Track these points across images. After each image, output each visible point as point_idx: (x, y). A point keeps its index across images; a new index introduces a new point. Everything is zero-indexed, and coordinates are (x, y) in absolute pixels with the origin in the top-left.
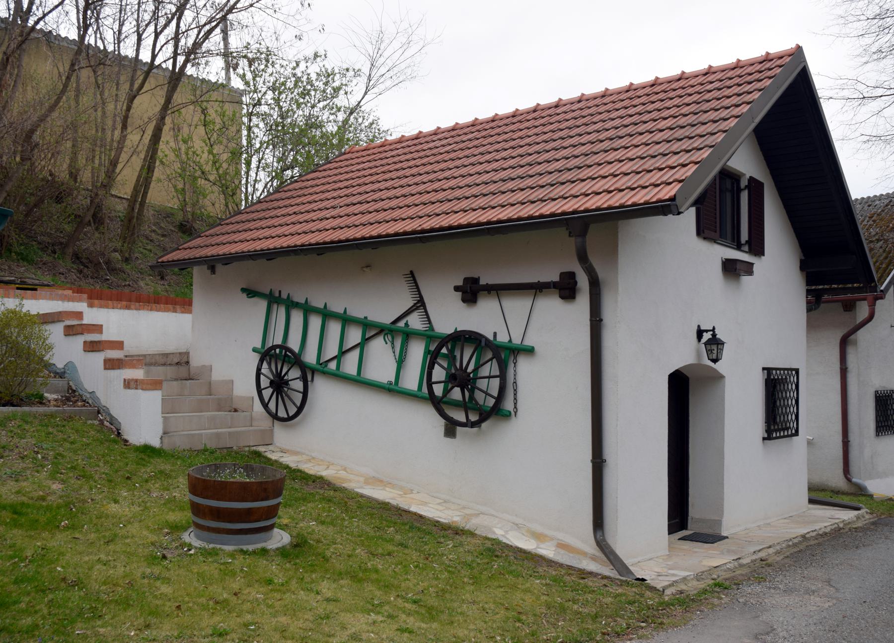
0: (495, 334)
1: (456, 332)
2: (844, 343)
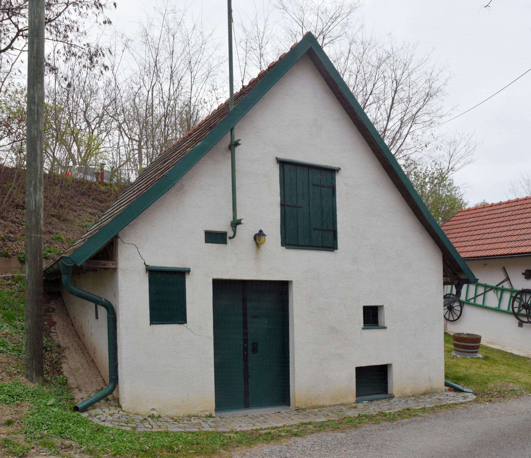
1: (523, 289)
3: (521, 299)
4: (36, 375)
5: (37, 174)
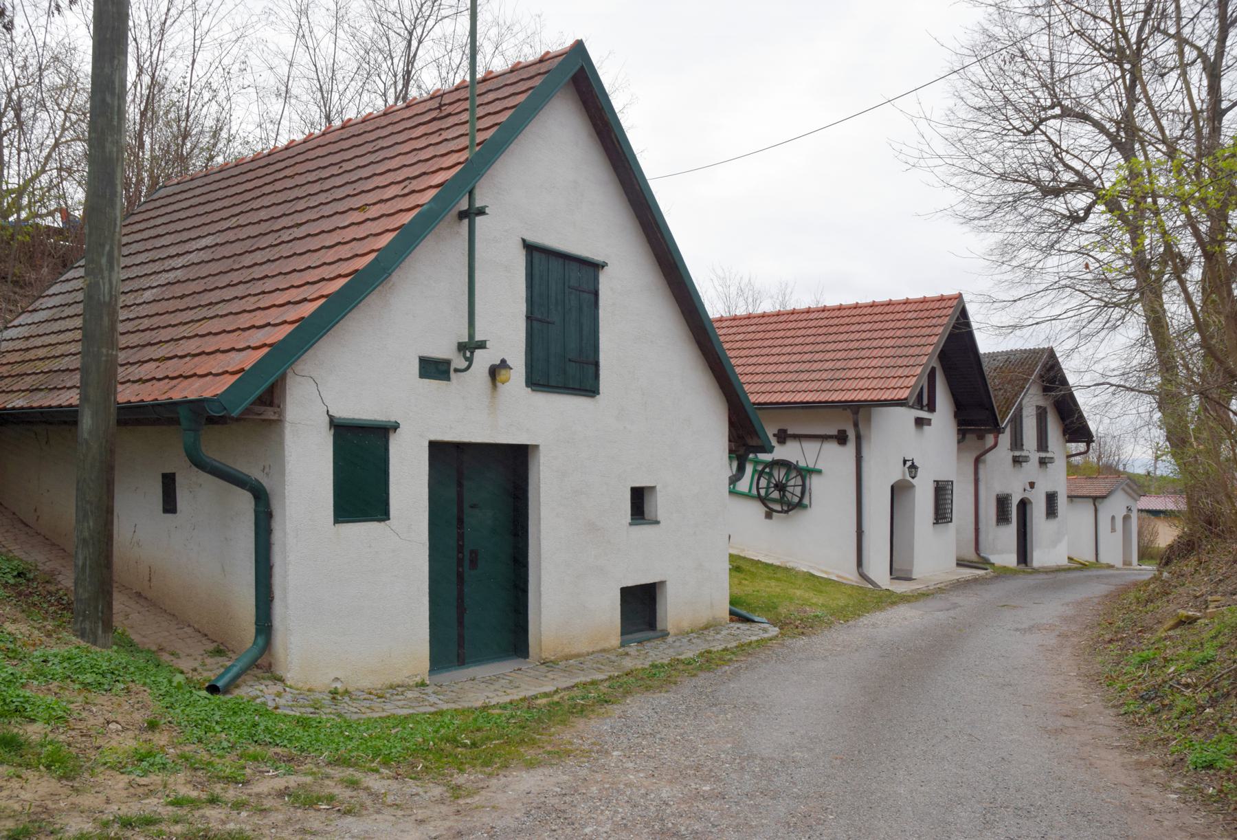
0: (797, 462)
1: (773, 460)
2: (977, 461)
3: (771, 475)
4: (103, 629)
5: (115, 232)
